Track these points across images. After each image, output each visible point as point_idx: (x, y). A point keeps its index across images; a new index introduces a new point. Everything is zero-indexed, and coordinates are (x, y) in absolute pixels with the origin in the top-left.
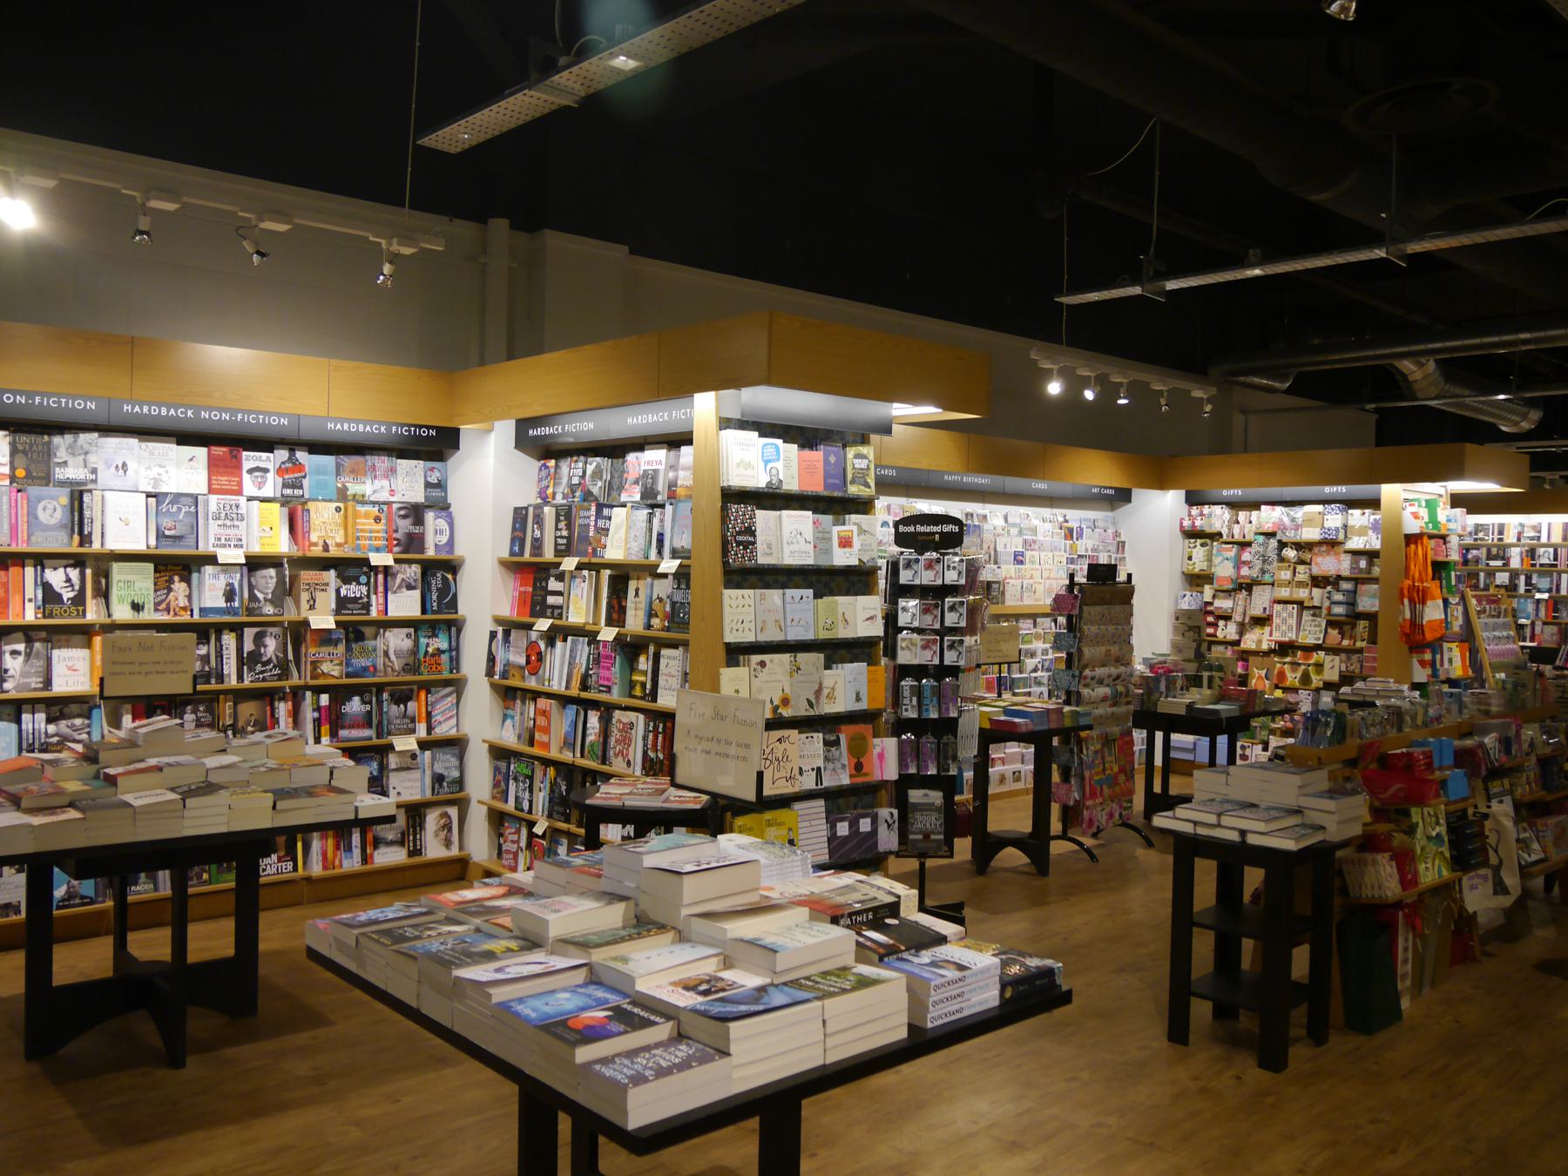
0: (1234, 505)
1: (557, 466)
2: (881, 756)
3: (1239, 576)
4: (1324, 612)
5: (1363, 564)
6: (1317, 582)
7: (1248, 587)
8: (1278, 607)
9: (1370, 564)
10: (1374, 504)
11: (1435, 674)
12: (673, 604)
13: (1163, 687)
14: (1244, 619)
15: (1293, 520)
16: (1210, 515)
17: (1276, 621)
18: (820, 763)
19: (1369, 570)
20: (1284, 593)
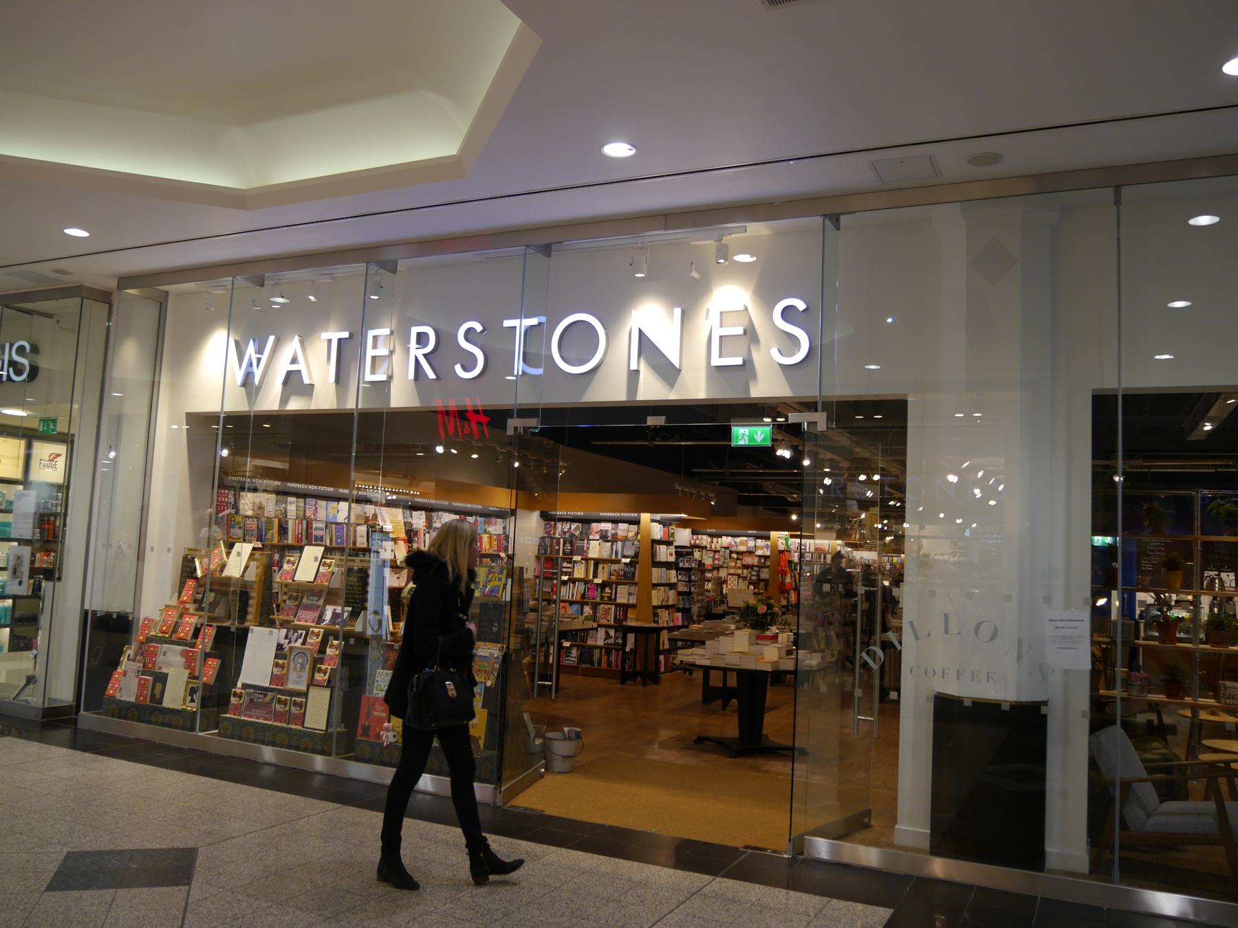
0: (711, 535)
1: (555, 524)
2: (677, 618)
3: (714, 564)
4: (748, 579)
5: (763, 561)
6: (745, 567)
7: (717, 568)
8: (730, 577)
9: (765, 561)
10: (768, 538)
11: (788, 602)
12: (625, 572)
13: (713, 604)
14: (745, 578)
15: (736, 543)
16: (701, 539)
17: (729, 582)
18: (667, 619)
19: (764, 563)
20: (732, 571)
